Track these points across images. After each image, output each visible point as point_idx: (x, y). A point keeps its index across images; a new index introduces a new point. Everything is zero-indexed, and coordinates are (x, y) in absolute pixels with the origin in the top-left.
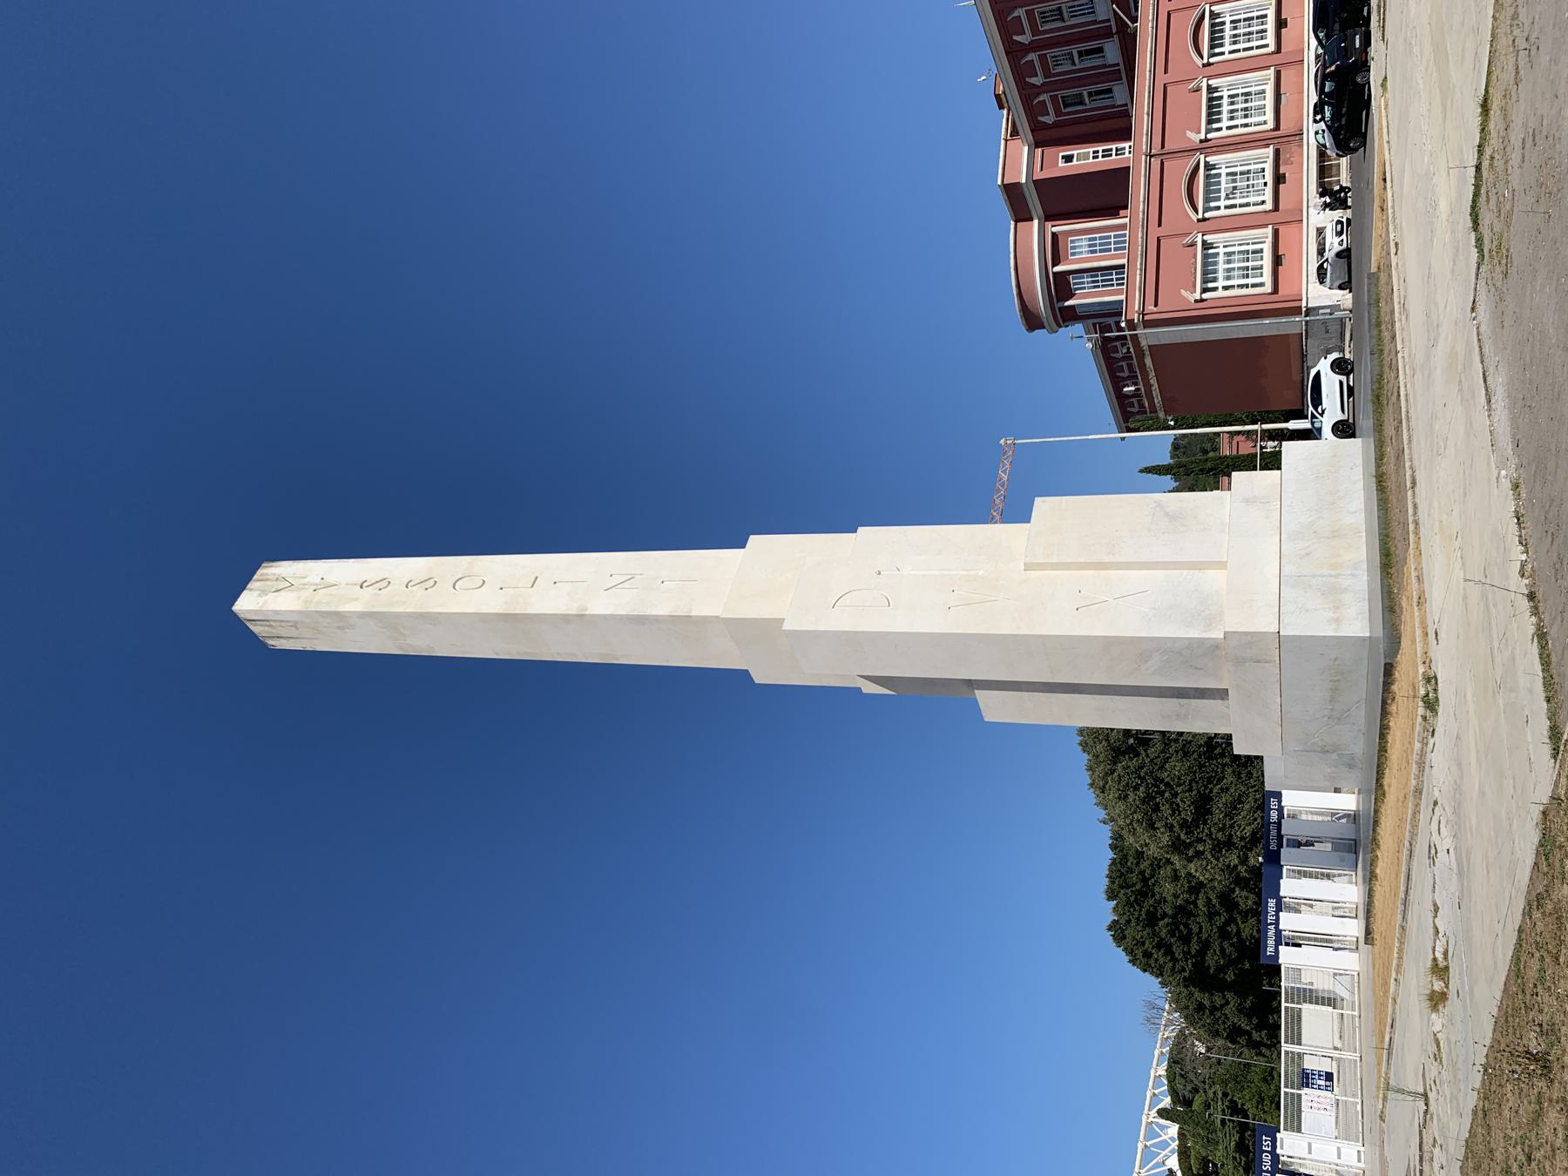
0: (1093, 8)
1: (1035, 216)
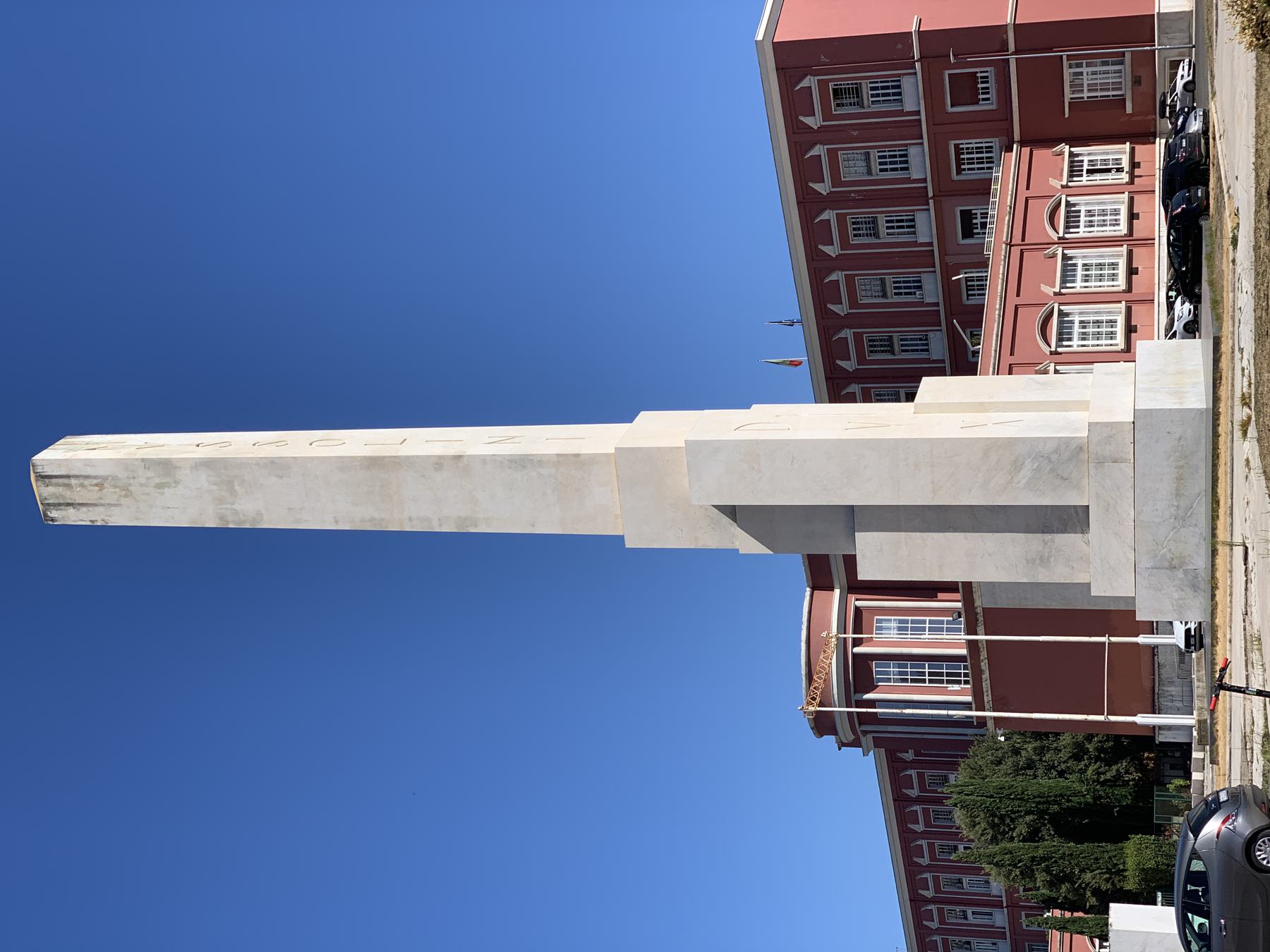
0: (927, 345)
1: (836, 584)
